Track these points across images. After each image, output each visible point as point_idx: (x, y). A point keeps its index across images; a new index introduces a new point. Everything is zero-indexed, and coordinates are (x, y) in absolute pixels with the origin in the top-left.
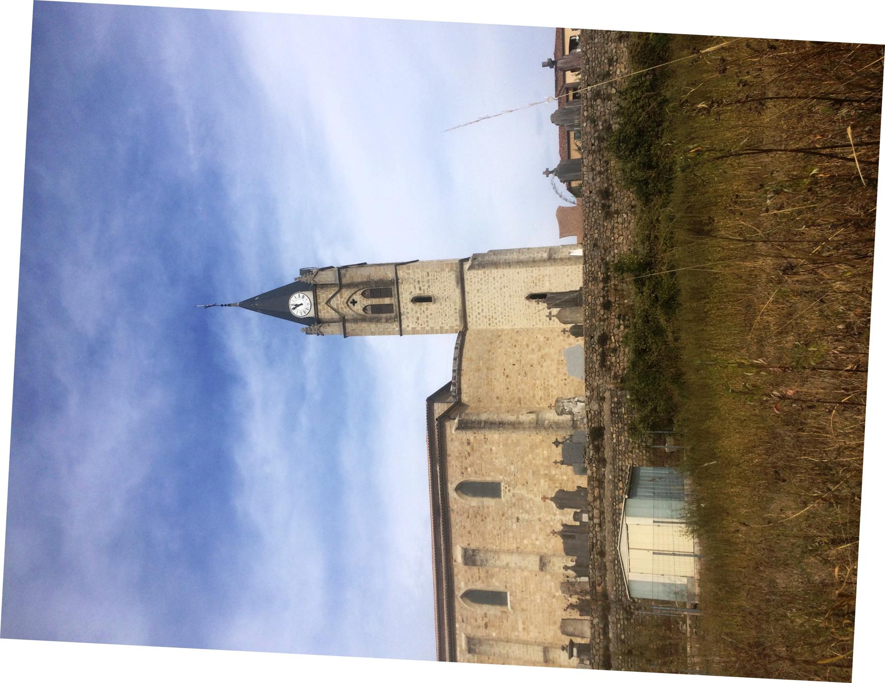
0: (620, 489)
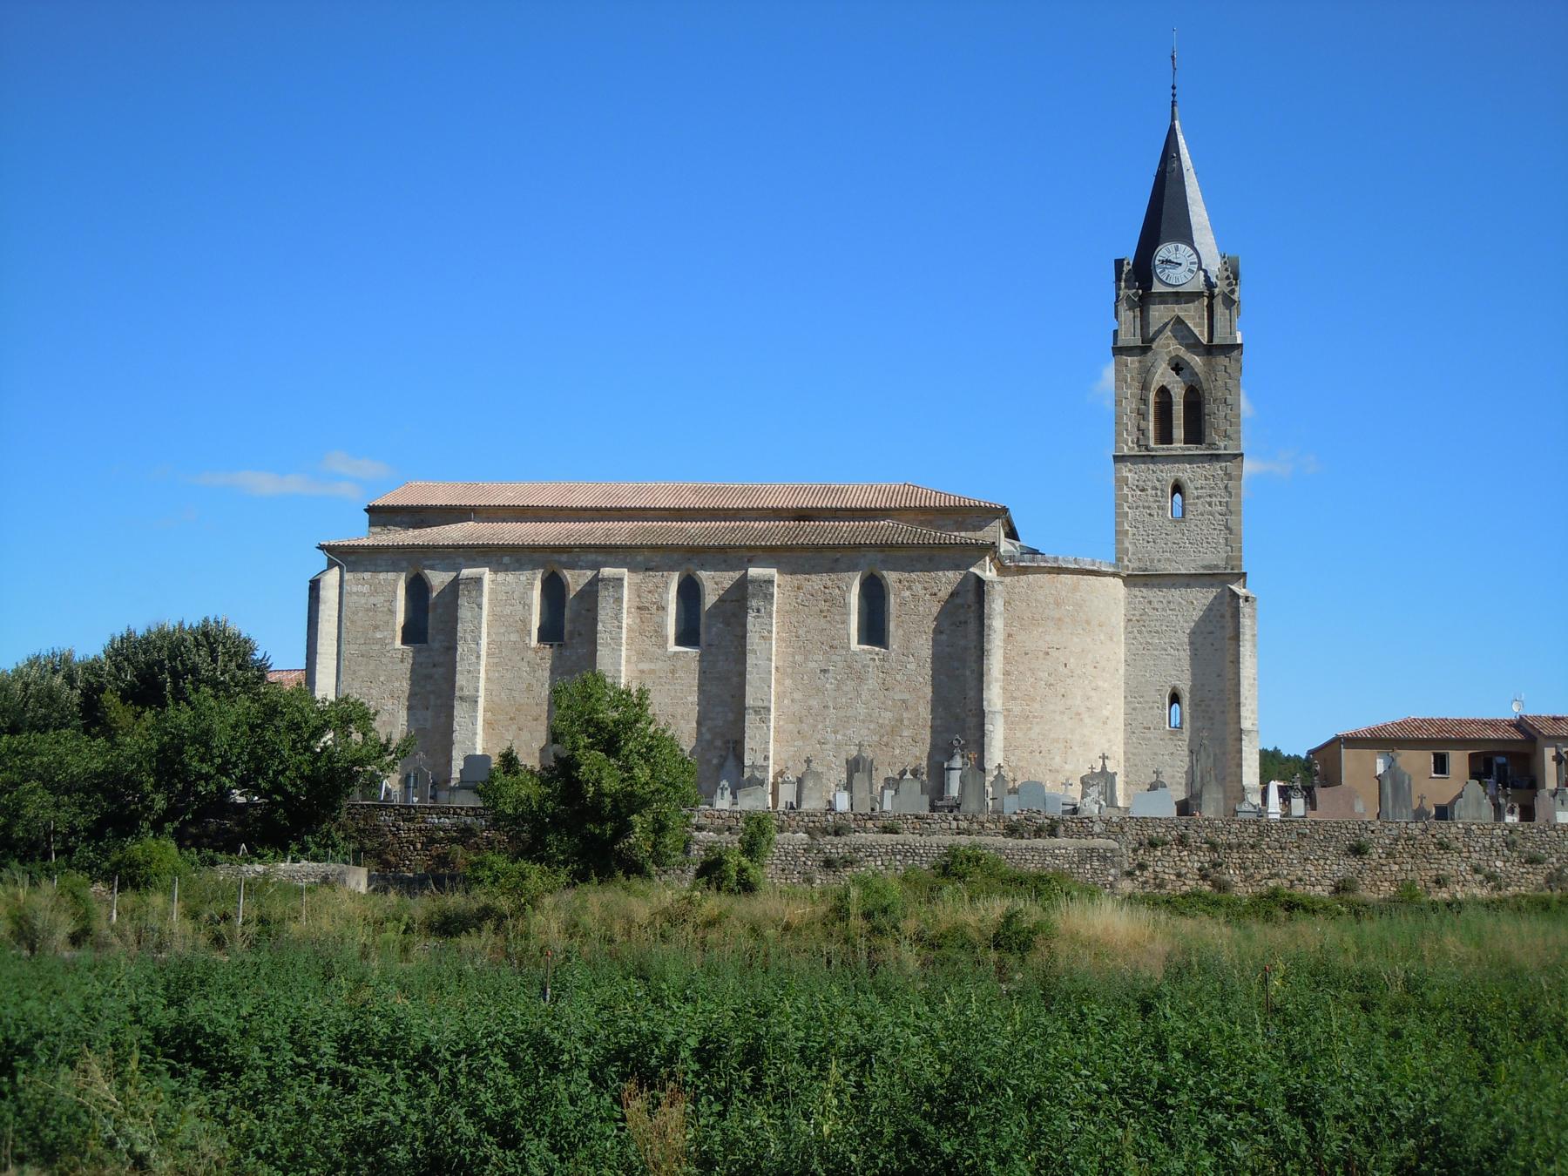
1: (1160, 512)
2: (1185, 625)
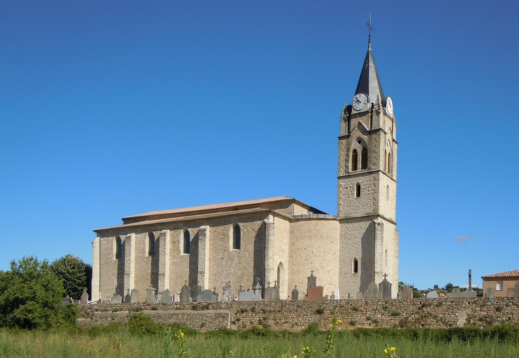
0: (187, 317)
1: (352, 196)
2: (359, 235)
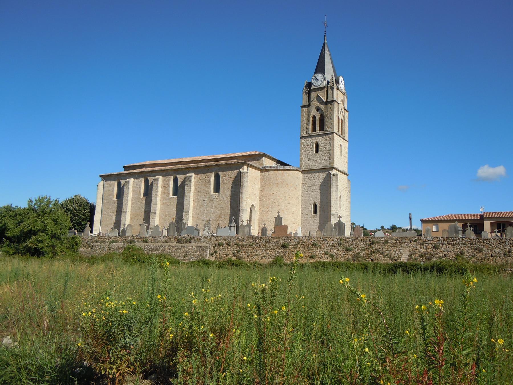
1: (312, 152)
2: (318, 184)
